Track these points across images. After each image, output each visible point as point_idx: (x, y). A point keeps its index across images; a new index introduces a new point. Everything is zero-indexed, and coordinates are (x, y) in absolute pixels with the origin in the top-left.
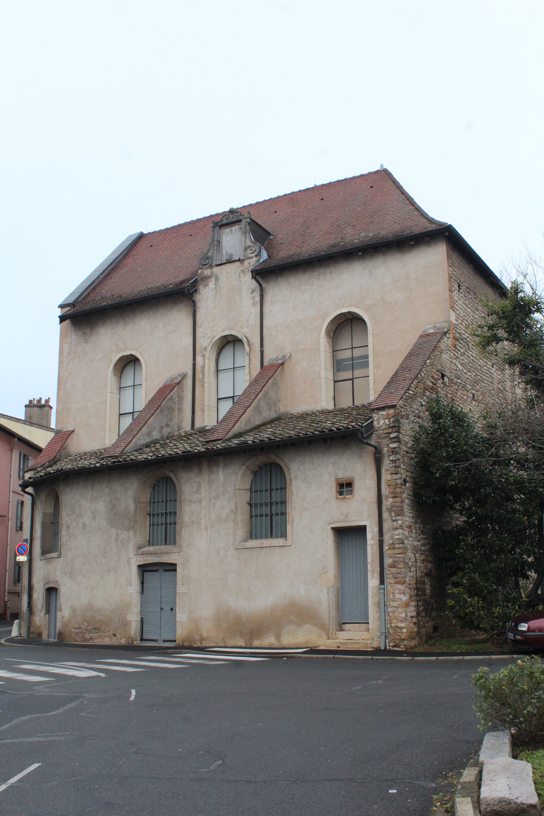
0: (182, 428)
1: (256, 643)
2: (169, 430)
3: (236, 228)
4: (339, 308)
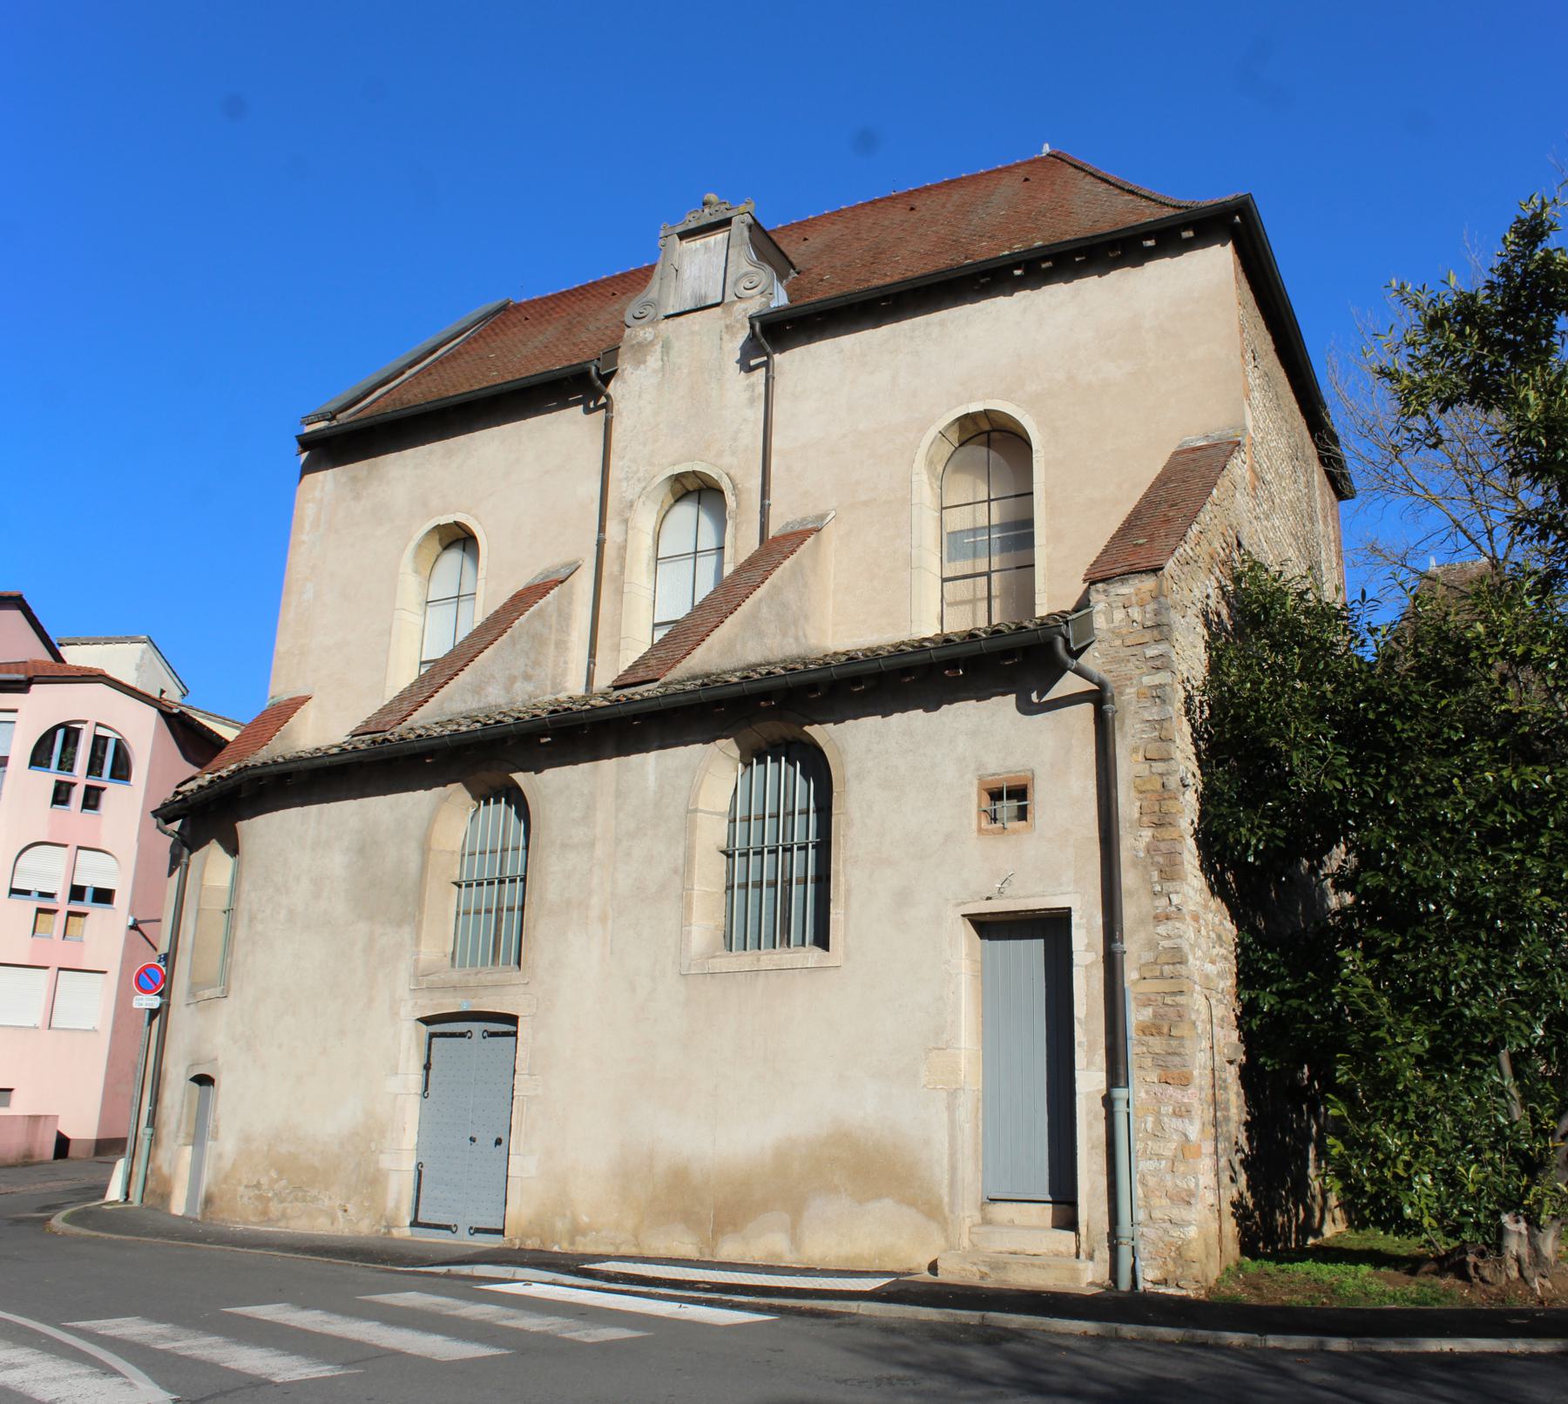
1: (729, 1250)
2: (530, 687)
3: (719, 237)
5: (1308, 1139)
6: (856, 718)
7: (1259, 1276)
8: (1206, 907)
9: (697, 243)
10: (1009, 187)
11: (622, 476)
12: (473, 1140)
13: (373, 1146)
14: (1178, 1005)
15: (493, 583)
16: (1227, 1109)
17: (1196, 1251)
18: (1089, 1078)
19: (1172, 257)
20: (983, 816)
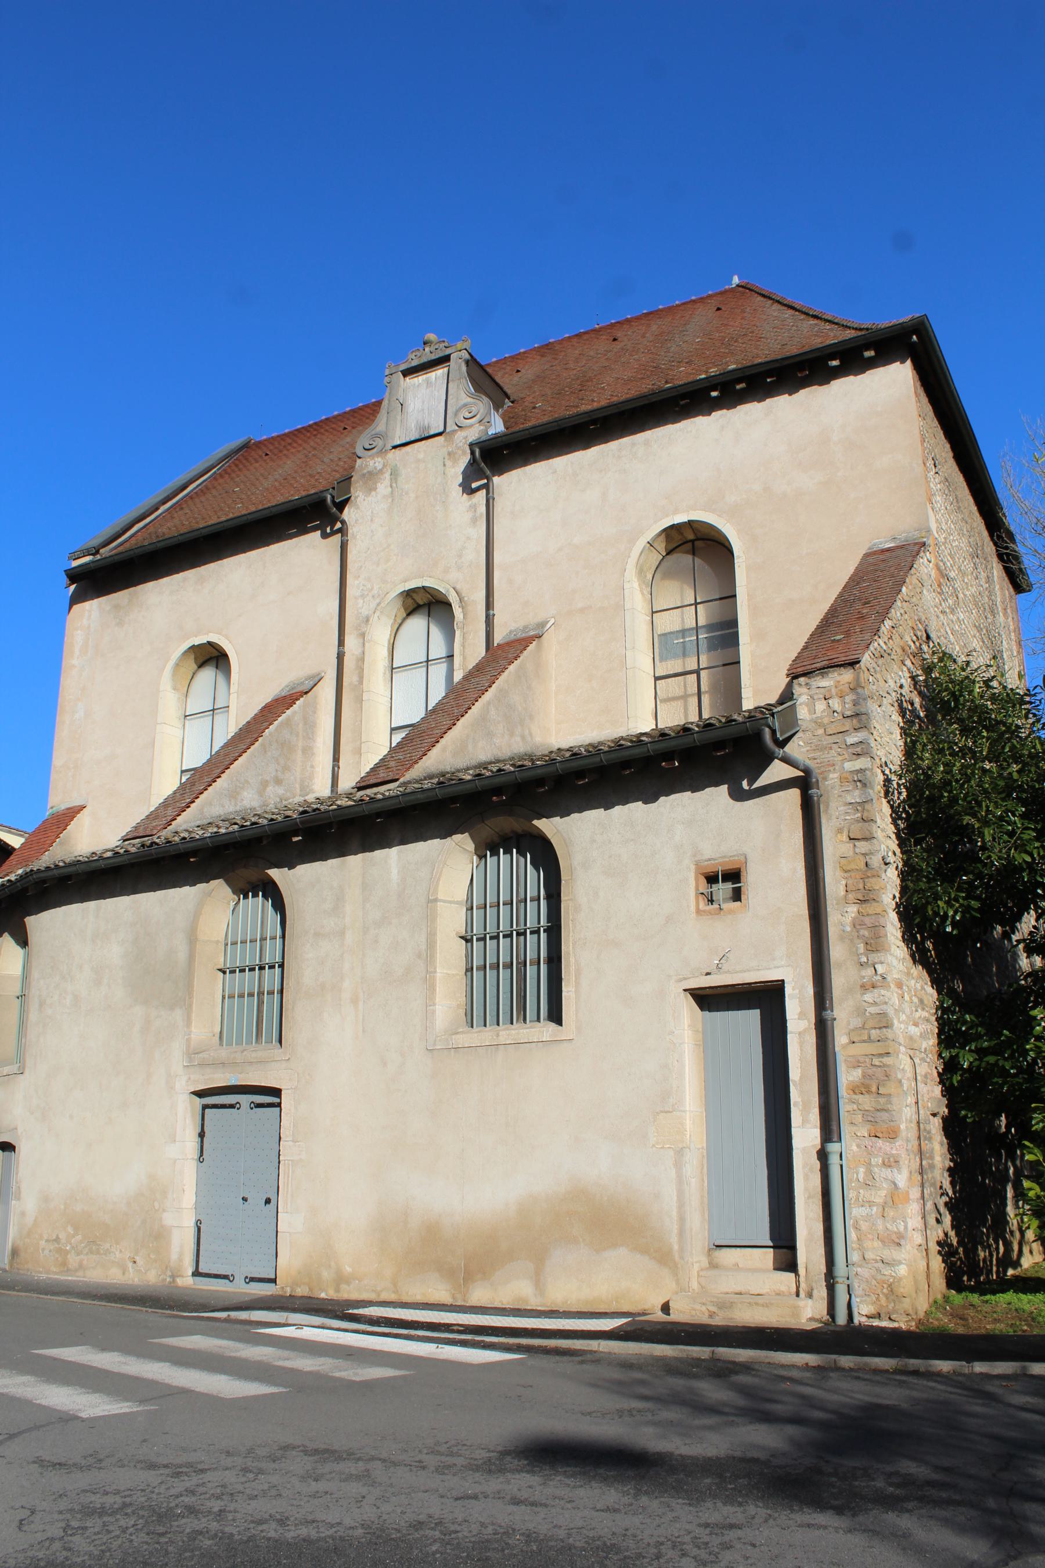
0: (312, 791)
1: (479, 1295)
2: (280, 791)
3: (440, 372)
5: (1005, 1179)
6: (580, 811)
7: (964, 1307)
8: (908, 974)
9: (420, 379)
10: (703, 316)
12: (245, 1199)
13: (156, 1204)
14: (885, 1065)
15: (244, 695)
16: (932, 1158)
17: (906, 1287)
18: (805, 1135)
19: (856, 375)
20: (701, 897)
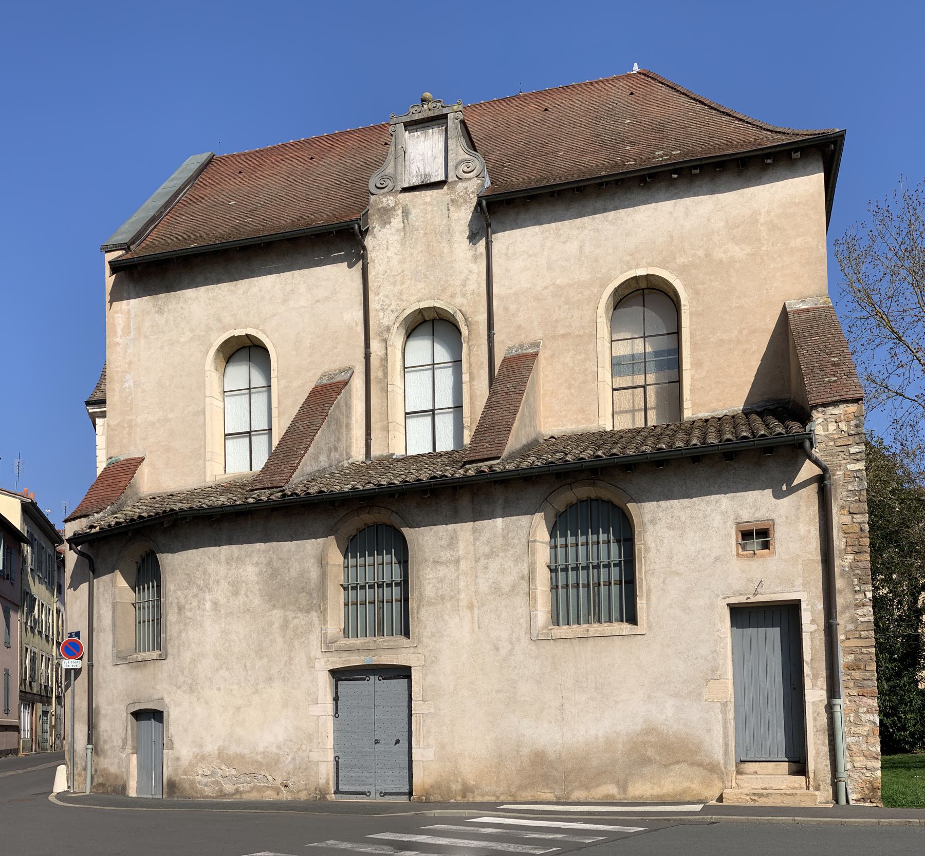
4: (631, 269)
11: (379, 307)
18: (815, 694)
